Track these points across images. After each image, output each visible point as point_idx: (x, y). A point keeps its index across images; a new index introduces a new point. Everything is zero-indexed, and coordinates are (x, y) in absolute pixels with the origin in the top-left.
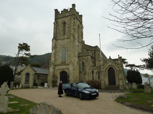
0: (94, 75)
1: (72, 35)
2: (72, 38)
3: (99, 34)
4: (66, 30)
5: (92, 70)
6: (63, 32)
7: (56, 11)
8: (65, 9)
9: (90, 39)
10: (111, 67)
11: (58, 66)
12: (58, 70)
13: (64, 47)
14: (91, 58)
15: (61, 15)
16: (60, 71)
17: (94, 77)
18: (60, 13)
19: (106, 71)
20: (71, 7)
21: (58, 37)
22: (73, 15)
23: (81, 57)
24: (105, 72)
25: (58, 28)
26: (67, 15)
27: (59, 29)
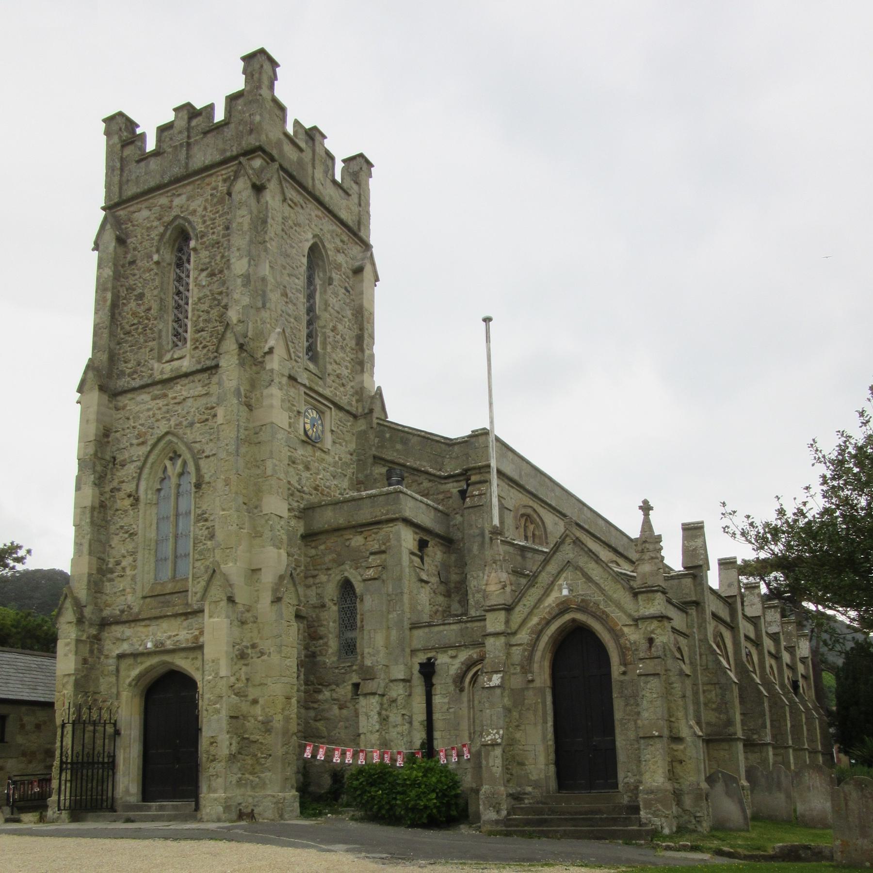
0: (437, 700)
1: (230, 345)
2: (229, 361)
3: (487, 320)
4: (194, 294)
5: (422, 658)
6: (171, 318)
7: (121, 130)
8: (188, 111)
9: (422, 383)
10: (580, 616)
11: (127, 631)
13: (175, 456)
14: (422, 545)
15: (153, 164)
16: (135, 673)
17: (436, 716)
18: (151, 145)
19: (530, 658)
20: (238, 83)
21: (128, 368)
22: (250, 153)
23: (332, 541)
24: (526, 666)
25: (131, 289)
26: (202, 156)
27: (141, 296)
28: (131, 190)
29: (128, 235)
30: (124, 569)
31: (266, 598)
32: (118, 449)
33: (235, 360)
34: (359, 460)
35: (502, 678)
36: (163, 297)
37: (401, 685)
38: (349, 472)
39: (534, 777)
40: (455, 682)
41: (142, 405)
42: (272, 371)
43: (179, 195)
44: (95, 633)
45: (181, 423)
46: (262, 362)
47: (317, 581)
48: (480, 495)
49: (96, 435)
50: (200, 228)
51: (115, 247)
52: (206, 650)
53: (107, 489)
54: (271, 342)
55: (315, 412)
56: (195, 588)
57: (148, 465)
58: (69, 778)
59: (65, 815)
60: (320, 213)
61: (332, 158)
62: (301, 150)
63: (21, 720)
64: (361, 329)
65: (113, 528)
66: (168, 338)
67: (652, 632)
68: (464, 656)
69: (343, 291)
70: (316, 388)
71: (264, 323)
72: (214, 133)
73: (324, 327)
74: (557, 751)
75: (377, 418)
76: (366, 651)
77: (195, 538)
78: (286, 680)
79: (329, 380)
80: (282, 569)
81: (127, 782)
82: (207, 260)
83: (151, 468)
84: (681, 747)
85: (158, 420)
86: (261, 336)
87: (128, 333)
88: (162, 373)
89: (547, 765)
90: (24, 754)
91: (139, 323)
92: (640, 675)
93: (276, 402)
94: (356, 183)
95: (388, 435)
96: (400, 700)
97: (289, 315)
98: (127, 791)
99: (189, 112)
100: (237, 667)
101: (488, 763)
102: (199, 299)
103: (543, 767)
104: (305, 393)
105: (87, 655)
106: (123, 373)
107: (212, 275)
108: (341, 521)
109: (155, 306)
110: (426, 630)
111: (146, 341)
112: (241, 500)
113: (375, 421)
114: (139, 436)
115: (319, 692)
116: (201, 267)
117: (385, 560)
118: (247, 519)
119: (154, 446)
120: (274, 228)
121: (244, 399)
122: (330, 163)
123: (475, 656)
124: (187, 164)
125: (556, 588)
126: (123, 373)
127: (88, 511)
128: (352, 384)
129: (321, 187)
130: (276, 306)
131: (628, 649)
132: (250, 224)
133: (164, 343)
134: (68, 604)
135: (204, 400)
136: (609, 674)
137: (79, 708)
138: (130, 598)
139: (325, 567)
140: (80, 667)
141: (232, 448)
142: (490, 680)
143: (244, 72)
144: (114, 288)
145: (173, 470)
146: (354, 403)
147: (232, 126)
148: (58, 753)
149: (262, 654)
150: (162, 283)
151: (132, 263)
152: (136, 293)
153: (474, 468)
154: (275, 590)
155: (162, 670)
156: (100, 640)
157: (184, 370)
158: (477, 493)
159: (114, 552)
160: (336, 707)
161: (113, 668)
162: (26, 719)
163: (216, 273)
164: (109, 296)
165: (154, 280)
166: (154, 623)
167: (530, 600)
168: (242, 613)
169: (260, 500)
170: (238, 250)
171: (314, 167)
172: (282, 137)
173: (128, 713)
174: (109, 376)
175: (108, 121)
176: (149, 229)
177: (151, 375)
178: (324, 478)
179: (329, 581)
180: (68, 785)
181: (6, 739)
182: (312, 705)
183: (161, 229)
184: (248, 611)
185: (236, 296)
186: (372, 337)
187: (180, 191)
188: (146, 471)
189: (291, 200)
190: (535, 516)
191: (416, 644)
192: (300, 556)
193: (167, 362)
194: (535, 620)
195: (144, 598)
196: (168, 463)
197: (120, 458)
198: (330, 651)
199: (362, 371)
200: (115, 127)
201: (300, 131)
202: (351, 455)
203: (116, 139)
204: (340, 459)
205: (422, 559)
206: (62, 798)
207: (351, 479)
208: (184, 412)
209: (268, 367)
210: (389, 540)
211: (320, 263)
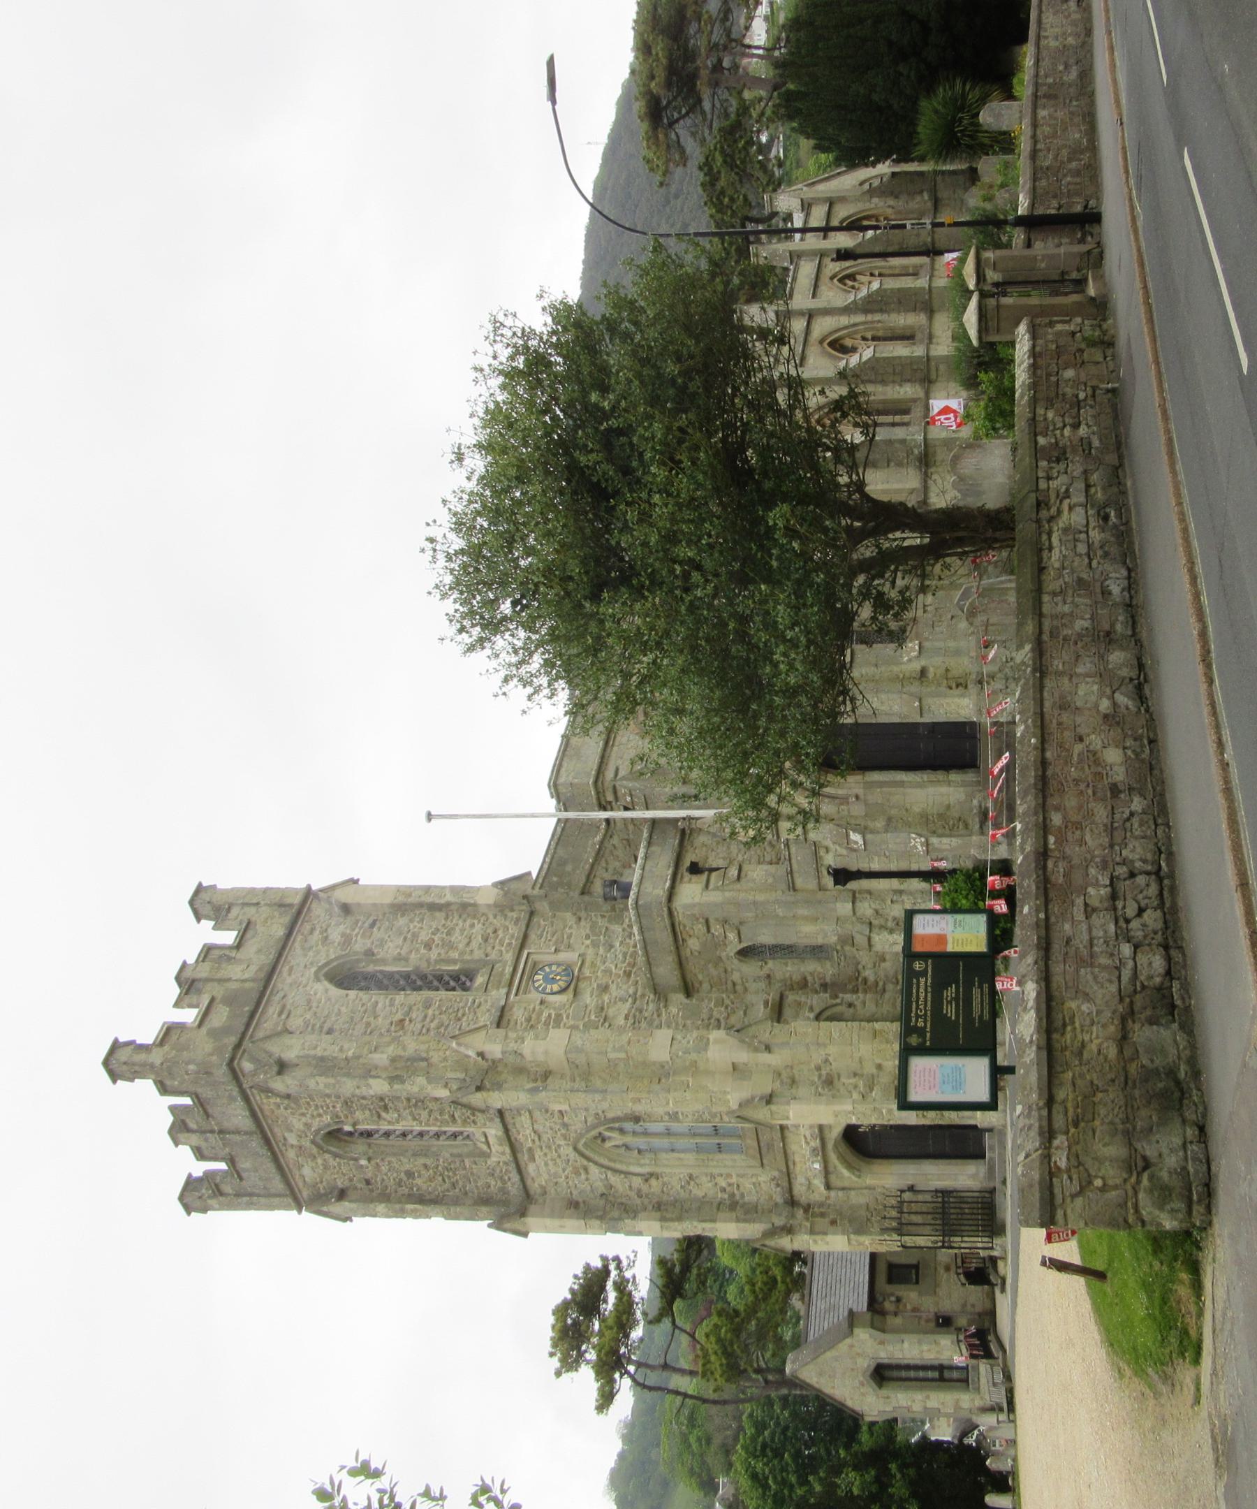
0: (876, 866)
1: (477, 1099)
2: (496, 1100)
3: (430, 817)
5: (829, 881)
7: (197, 1195)
12: (834, 1180)
15: (244, 1164)
16: (846, 1173)
22: (235, 1074)
26: (238, 1116)
27: (410, 1174)
28: (278, 1185)
29: (335, 1187)
30: (730, 1185)
31: (764, 1058)
32: (592, 1191)
33: (496, 1094)
34: (586, 909)
35: (854, 831)
36: (410, 1153)
37: (858, 904)
38: (601, 922)
39: (963, 797)
41: (540, 1171)
42: (503, 1053)
43: (285, 1139)
44: (801, 1211)
46: (494, 1062)
47: (739, 981)
48: (631, 795)
49: (578, 1218)
50: (327, 1119)
51: (350, 1201)
52: (824, 1122)
53: (638, 1201)
54: (471, 1053)
55: (537, 977)
57: (612, 1165)
58: (959, 1239)
59: (997, 1241)
60: (286, 969)
61: (208, 950)
62: (213, 1000)
64: (421, 905)
65: (683, 1194)
66: (459, 1145)
70: (508, 976)
71: (445, 1059)
72: (208, 1107)
74: (934, 767)
75: (533, 888)
77: (697, 1121)
78: (855, 1037)
79: (493, 956)
80: (732, 1041)
81: (962, 1176)
82: (367, 1112)
84: (931, 669)
85: (559, 1156)
86: (461, 1063)
87: (454, 1186)
89: (949, 783)
93: (540, 1046)
94: (229, 910)
95: (555, 879)
96: (875, 905)
97: (426, 1017)
98: (974, 1176)
99: (181, 1132)
100: (842, 1089)
102: (415, 1119)
103: (951, 789)
104: (516, 995)
105: (827, 1220)
106: (503, 1190)
108: (671, 959)
109: (422, 1161)
110: (796, 875)
111: (465, 1168)
112: (656, 1087)
113: (537, 891)
114: (577, 1173)
115: (865, 980)
116: (375, 1118)
117: (717, 920)
118: (677, 1078)
119: (589, 1159)
120: (326, 1047)
121: (539, 1083)
122: (216, 953)
124: (246, 1133)
126: (503, 1190)
128: (491, 917)
129: (253, 968)
130: (423, 1043)
132: (327, 1077)
133: (466, 1150)
134: (771, 1243)
137: (884, 1230)
138: (761, 1179)
139: (723, 975)
140: (840, 1228)
141: (597, 1097)
143: (132, 1080)
144: (400, 1202)
146: (515, 915)
147: (199, 1090)
149: (826, 1061)
150: (394, 1155)
151: (368, 1182)
153: (598, 799)
154: (756, 1050)
155: (843, 1148)
156: (809, 1205)
157: (500, 1133)
158: (629, 799)
159: (711, 1193)
160: (883, 964)
161: (840, 1193)
163: (382, 1104)
164: (409, 1207)
165: (389, 1162)
166: (791, 1158)
168: (782, 1083)
169: (654, 1063)
171: (229, 980)
172: (204, 1030)
173: (889, 1177)
174: (505, 1203)
175: (188, 1209)
176: (326, 1167)
177: (505, 1163)
178: (614, 962)
179: (739, 970)
180: (966, 1239)
181: (914, 1262)
184: (780, 1075)
185: (415, 1089)
186: (427, 889)
188: (618, 1166)
191: (812, 885)
195: (762, 1165)
196: (608, 1144)
197: (602, 1189)
198: (819, 969)
199: (475, 905)
200: (198, 1203)
201: (187, 999)
202: (580, 919)
203: (212, 1202)
204: (588, 937)
205: (712, 870)
209: (500, 1056)
210: (694, 915)
211: (348, 966)
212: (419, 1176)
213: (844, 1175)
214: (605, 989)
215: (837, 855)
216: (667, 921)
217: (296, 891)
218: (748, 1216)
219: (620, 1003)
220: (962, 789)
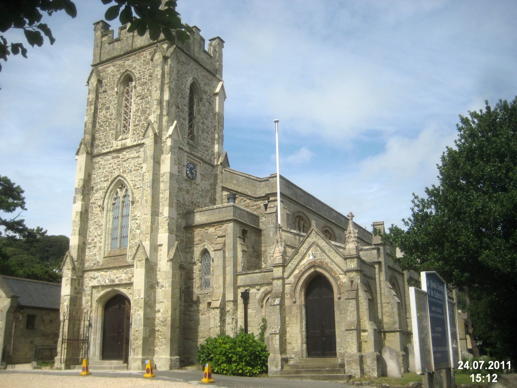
0: (249, 311)
16: (102, 293)
25: (104, 104)
27: (108, 108)
28: (104, 59)
30: (96, 243)
32: (95, 183)
40: (259, 302)
43: (128, 60)
45: (125, 170)
50: (138, 75)
51: (97, 85)
56: (130, 253)
57: (109, 191)
60: (197, 67)
61: (203, 40)
63: (43, 318)
67: (353, 277)
68: (263, 289)
69: (208, 104)
73: (198, 122)
76: (215, 286)
83: (111, 193)
85: (114, 169)
87: (101, 126)
88: (117, 146)
89: (302, 344)
90: (43, 335)
91: (107, 121)
92: (346, 299)
101: (272, 343)
102: (136, 110)
103: (300, 345)
105: (77, 286)
107: (142, 99)
111: (110, 130)
114: (105, 177)
123: (269, 289)
125: (307, 255)
127: (79, 214)
131: (342, 286)
135: (137, 160)
136: (333, 298)
142: (274, 301)
145: (121, 194)
148: (61, 334)
150: (118, 102)
152: (105, 106)
155: (114, 294)
162: (45, 317)
167: (295, 262)
170: (155, 87)
180: (66, 350)
182: (187, 313)
183: (119, 76)
187: (129, 58)
189: (182, 62)
190: (304, 217)
192: (183, 237)
193: (120, 140)
194: (297, 272)
195: (106, 257)
196: (118, 190)
204: (205, 188)
206: (62, 357)
207: (210, 198)
208: (127, 165)
210: (227, 230)
211: (196, 91)
212: (107, 112)
213: (98, 294)
214: (188, 192)
215: (256, 294)
216: (224, 219)
217: (221, 77)
218: (80, 250)
219: (182, 198)
220: (300, 349)
